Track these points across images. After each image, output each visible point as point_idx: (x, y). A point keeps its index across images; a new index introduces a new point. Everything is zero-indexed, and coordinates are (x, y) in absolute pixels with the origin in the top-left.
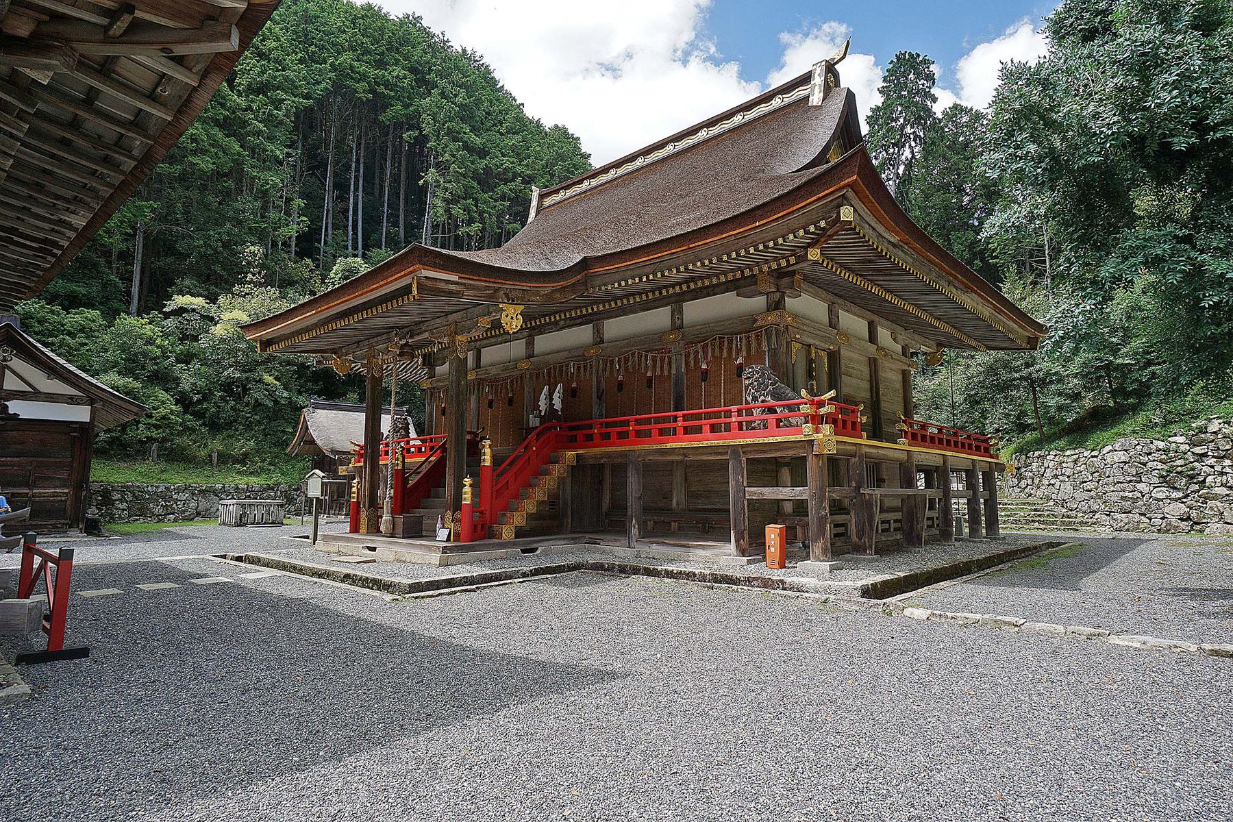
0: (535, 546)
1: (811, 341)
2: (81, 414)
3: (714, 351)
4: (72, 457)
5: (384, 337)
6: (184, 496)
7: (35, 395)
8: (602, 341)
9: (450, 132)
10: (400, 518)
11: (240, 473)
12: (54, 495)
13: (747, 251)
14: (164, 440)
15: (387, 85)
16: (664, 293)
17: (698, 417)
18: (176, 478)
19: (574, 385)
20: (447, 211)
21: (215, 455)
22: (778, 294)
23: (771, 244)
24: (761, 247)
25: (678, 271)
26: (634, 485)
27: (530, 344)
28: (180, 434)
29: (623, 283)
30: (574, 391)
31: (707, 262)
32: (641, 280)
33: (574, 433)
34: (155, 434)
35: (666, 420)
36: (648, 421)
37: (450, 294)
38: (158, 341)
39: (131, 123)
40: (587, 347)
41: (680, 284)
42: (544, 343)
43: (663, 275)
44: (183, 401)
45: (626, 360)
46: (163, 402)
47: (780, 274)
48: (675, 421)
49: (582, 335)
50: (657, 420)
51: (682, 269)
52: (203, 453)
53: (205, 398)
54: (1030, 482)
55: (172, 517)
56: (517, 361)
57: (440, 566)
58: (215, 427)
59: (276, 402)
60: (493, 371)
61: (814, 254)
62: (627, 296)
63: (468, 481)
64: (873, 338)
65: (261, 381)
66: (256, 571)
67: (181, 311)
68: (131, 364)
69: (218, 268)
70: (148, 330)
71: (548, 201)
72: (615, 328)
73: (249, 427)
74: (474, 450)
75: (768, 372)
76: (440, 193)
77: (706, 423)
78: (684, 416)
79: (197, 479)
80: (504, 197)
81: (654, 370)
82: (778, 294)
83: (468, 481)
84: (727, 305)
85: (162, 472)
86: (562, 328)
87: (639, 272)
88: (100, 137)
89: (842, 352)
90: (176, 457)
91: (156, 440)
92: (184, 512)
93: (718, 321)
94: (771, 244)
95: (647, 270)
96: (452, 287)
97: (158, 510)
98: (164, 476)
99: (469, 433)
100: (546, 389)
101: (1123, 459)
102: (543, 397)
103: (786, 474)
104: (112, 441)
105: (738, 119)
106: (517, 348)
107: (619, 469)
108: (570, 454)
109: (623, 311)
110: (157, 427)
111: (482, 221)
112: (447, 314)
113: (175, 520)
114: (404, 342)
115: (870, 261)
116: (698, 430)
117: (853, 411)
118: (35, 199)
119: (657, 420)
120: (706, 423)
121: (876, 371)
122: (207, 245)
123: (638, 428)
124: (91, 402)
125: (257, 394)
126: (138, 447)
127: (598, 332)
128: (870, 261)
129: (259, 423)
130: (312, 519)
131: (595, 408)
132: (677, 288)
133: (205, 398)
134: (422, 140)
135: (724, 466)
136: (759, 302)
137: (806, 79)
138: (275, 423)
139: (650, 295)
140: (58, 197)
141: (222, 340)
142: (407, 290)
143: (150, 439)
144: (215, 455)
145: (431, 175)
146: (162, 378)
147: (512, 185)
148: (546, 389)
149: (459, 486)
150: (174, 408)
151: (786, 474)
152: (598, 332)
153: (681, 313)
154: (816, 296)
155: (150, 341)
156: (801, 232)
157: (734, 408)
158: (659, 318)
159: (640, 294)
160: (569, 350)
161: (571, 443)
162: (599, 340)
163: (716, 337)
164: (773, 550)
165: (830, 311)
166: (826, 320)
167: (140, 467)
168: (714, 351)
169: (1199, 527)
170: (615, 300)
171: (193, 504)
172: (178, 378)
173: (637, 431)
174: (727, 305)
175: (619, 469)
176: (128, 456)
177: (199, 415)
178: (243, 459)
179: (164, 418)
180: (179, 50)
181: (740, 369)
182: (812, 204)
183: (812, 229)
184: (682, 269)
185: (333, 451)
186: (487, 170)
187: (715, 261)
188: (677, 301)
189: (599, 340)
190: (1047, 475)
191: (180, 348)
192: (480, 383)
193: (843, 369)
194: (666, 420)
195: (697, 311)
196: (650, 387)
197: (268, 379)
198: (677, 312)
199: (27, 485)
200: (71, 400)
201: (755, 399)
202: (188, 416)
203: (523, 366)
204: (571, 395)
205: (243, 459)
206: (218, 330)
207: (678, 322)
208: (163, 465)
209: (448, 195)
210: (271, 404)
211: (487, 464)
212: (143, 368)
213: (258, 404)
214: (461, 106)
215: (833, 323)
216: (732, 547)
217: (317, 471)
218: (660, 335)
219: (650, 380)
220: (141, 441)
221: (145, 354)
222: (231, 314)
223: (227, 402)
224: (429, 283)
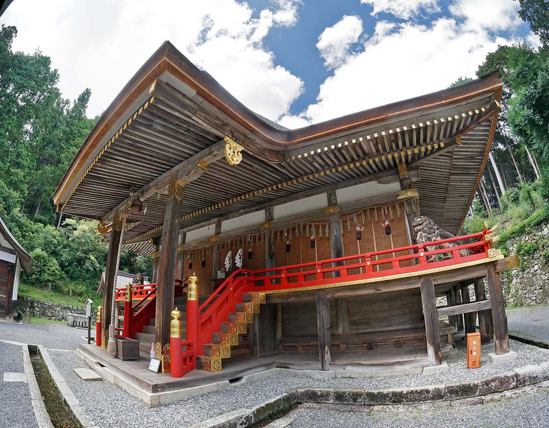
3: (385, 212)
8: (272, 219)
11: (79, 301)
14: (53, 282)
18: (56, 300)
19: (250, 250)
21: (71, 291)
30: (250, 255)
34: (51, 278)
38: (57, 237)
40: (262, 225)
44: (62, 265)
45: (294, 229)
46: (54, 264)
49: (257, 217)
52: (66, 290)
55: (54, 318)
58: (72, 278)
59: (94, 269)
60: (193, 245)
63: (176, 313)
65: (90, 259)
68: (46, 246)
70: (55, 233)
72: (281, 211)
73: (84, 280)
74: (180, 291)
79: (63, 301)
81: (317, 233)
83: (176, 313)
85: (52, 296)
86: (241, 214)
90: (57, 289)
91: (50, 281)
92: (58, 316)
97: (49, 314)
98: (52, 298)
100: (229, 254)
102: (227, 259)
104: (37, 279)
107: (309, 307)
108: (262, 294)
110: (51, 275)
113: (55, 320)
125: (87, 264)
126: (44, 283)
129: (88, 279)
131: (268, 266)
138: (94, 280)
141: (77, 238)
143: (49, 280)
144: (71, 291)
146: (54, 253)
148: (229, 254)
150: (57, 267)
153: (335, 195)
155: (54, 237)
158: (319, 200)
161: (259, 285)
162: (270, 218)
167: (45, 292)
168: (385, 212)
171: (61, 313)
172: (62, 255)
175: (309, 307)
176: (42, 287)
177: (67, 272)
178: (80, 294)
179: (53, 271)
189: (270, 218)
192: (184, 253)
195: (346, 194)
196: (313, 247)
197: (92, 258)
202: (63, 272)
204: (248, 257)
205: (80, 294)
206: (76, 233)
208: (52, 293)
210: (92, 270)
212: (50, 248)
213: (88, 270)
218: (321, 211)
219: (313, 242)
220: (46, 282)
223: (77, 268)
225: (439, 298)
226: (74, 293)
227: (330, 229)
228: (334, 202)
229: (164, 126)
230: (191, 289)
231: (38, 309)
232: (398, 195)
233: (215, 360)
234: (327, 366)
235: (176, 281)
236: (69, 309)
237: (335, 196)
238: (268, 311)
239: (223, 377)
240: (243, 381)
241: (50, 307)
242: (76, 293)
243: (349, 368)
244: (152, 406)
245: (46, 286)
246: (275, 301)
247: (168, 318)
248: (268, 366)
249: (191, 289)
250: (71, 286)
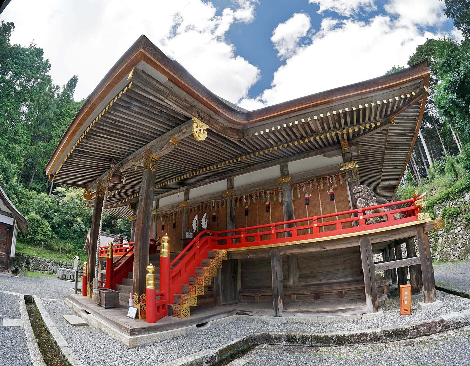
3: (329, 181)
8: (233, 187)
11: (68, 257)
14: (46, 241)
18: (48, 257)
19: (214, 214)
21: (61, 249)
30: (214, 218)
34: (43, 238)
38: (49, 203)
40: (224, 192)
44: (53, 227)
45: (251, 196)
46: (46, 226)
49: (220, 186)
52: (56, 248)
55: (46, 272)
57: (130, 347)
58: (62, 238)
59: (81, 230)
60: (165, 209)
63: (150, 268)
65: (77, 221)
68: (39, 210)
70: (47, 199)
72: (241, 180)
73: (72, 239)
74: (154, 249)
79: (54, 258)
81: (272, 199)
83: (150, 268)
85: (44, 253)
86: (207, 183)
90: (49, 247)
91: (43, 240)
92: (50, 270)
97: (42, 268)
98: (44, 255)
99: (151, 240)
100: (196, 217)
102: (194, 221)
104: (32, 239)
107: (265, 263)
110: (44, 235)
113: (47, 273)
125: (75, 226)
126: (38, 242)
129: (76, 238)
131: (229, 227)
138: (80, 239)
141: (66, 203)
143: (42, 240)
144: (61, 249)
146: (46, 217)
148: (196, 217)
149: (144, 272)
150: (49, 228)
153: (287, 167)
155: (46, 202)
158: (273, 171)
161: (222, 244)
162: (231, 186)
167: (39, 250)
168: (329, 181)
171: (52, 268)
172: (53, 218)
173: (246, 238)
175: (265, 263)
176: (36, 245)
177: (57, 233)
178: (69, 252)
179: (46, 232)
189: (231, 186)
192: (158, 216)
195: (296, 166)
196: (268, 211)
197: (79, 220)
202: (54, 233)
204: (212, 219)
205: (69, 252)
206: (65, 199)
208: (45, 251)
210: (79, 230)
212: (43, 212)
213: (75, 231)
218: (275, 181)
219: (268, 207)
220: (40, 241)
223: (66, 229)
225: (376, 255)
226: (63, 251)
227: (282, 196)
228: (286, 172)
229: (141, 108)
230: (163, 248)
231: (32, 265)
232: (341, 167)
234: (280, 313)
236: (59, 264)
237: (287, 167)
240: (208, 326)
241: (43, 263)
242: (65, 250)
243: (299, 314)
245: (40, 244)
246: (235, 257)
248: (230, 313)
249: (163, 248)
250: (61, 245)
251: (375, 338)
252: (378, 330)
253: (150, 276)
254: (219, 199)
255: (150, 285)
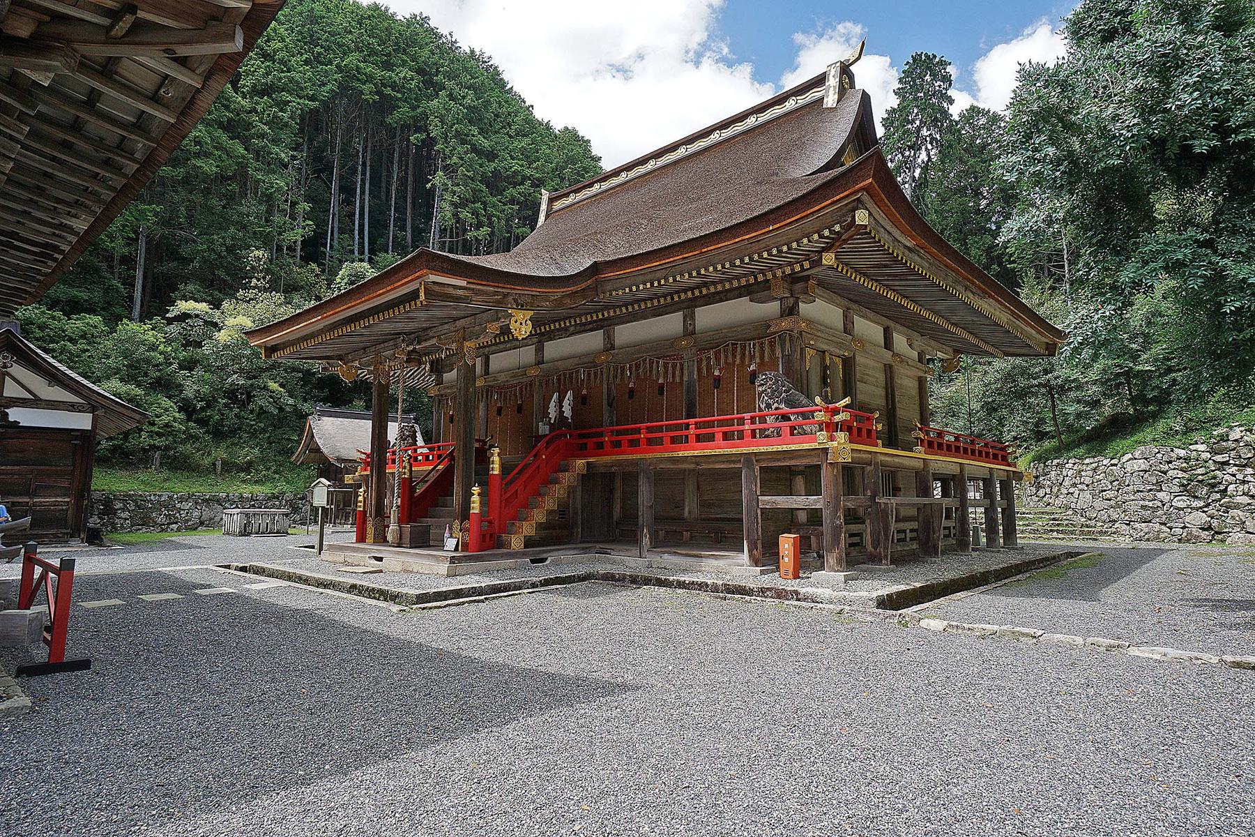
0: (544, 556)
1: (825, 347)
2: (83, 422)
3: (726, 357)
4: (74, 465)
5: (391, 343)
6: (187, 505)
7: (35, 402)
8: (613, 347)
9: (458, 134)
10: (407, 528)
11: (244, 481)
12: (55, 504)
13: (760, 256)
14: (167, 448)
15: (394, 86)
16: (676, 299)
17: (710, 424)
18: (180, 487)
19: (584, 392)
20: (455, 215)
21: (219, 464)
22: (792, 300)
23: (785, 248)
24: (775, 252)
25: (690, 276)
26: (645, 494)
27: (540, 350)
28: (183, 442)
29: (634, 288)
30: (584, 398)
31: (719, 267)
32: (652, 285)
33: (585, 441)
34: (158, 442)
35: (678, 427)
36: (660, 429)
37: (458, 299)
38: (161, 347)
39: (134, 125)
40: (598, 354)
41: (692, 289)
42: (554, 349)
43: (675, 280)
44: (187, 408)
45: (638, 366)
46: (166, 410)
47: (794, 279)
48: (687, 428)
49: (592, 341)
50: (669, 428)
51: (694, 274)
52: (207, 461)
53: (209, 406)
54: (1048, 490)
55: (175, 526)
56: (526, 367)
58: (219, 434)
59: (281, 409)
60: (502, 378)
61: (829, 259)
62: (638, 301)
63: (476, 490)
64: (888, 344)
65: (265, 388)
66: (260, 581)
67: (184, 317)
68: (134, 371)
69: (221, 273)
70: (150, 336)
71: (558, 205)
72: (626, 333)
73: (253, 435)
74: (482, 458)
75: (782, 379)
76: (447, 196)
77: (718, 431)
78: (696, 423)
79: (201, 488)
80: (513, 201)
81: (666, 377)
82: (792, 300)
83: (476, 490)
84: (740, 310)
85: (165, 480)
86: (572, 334)
87: (650, 276)
88: (101, 139)
89: (857, 358)
90: (179, 465)
91: (158, 448)
92: (187, 521)
93: (731, 327)
94: (785, 248)
95: (659, 275)
96: (460, 292)
97: (161, 519)
98: (167, 485)
100: (555, 396)
101: (1143, 467)
102: (552, 404)
103: (800, 482)
104: (114, 449)
105: (751, 121)
106: (527, 355)
108: (580, 462)
109: (634, 317)
110: (159, 435)
111: (490, 225)
112: (455, 319)
113: (179, 530)
114: (411, 348)
115: (885, 266)
116: (711, 438)
117: (868, 419)
118: (36, 202)
119: (669, 428)
120: (718, 431)
121: (892, 378)
122: (210, 250)
123: (650, 435)
124: (93, 409)
125: (261, 401)
126: (140, 455)
127: (609, 338)
128: (885, 266)
129: (264, 430)
130: (317, 528)
131: (606, 416)
132: (689, 294)
133: (209, 406)
134: (430, 142)
135: (736, 474)
136: (773, 308)
137: (820, 80)
138: (280, 431)
139: (662, 301)
140: (59, 201)
141: (226, 347)
142: (414, 295)
143: (153, 447)
144: (219, 464)
145: (439, 178)
146: (165, 385)
147: (521, 188)
148: (555, 396)
150: (177, 415)
151: (800, 482)
152: (609, 338)
153: (693, 318)
154: (830, 301)
155: (153, 348)
156: (816, 237)
157: (747, 416)
158: (671, 324)
159: (651, 299)
160: (579, 356)
161: (582, 451)
162: (610, 346)
163: (729, 343)
164: (786, 560)
165: (845, 316)
166: (841, 326)
167: (143, 475)
168: (726, 357)
169: (1220, 537)
170: (626, 306)
171: (196, 513)
172: (181, 385)
173: (648, 439)
174: (740, 310)
176: (131, 464)
177: (202, 423)
178: (247, 467)
179: (167, 425)
180: (183, 51)
181: (753, 376)
182: (826, 207)
183: (826, 233)
184: (694, 274)
185: (339, 460)
186: (496, 173)
187: (727, 265)
188: (689, 307)
189: (610, 346)
190: (1066, 483)
191: (183, 354)
192: (489, 390)
193: (858, 375)
194: (678, 427)
195: (709, 317)
196: (662, 394)
197: (273, 386)
198: (689, 317)
199: (27, 494)
200: (72, 407)
201: (769, 406)
202: (191, 424)
203: (532, 372)
204: (581, 402)
205: (247, 467)
206: (222, 336)
207: (690, 328)
208: (166, 474)
209: (456, 199)
210: (276, 412)
211: (496, 472)
212: (146, 375)
213: (262, 412)
214: (469, 108)
215: (848, 329)
216: (745, 557)
217: (323, 480)
218: (672, 341)
219: (661, 387)
220: (143, 449)
221: (148, 361)
222: (235, 320)
223: (231, 409)
224: (437, 288)
233: (516, 542)
235: (477, 441)
238: (590, 476)
239: (524, 555)
244: (448, 576)
247: (468, 495)
251: (715, 589)
252: (720, 582)
253: (476, 498)
254: (589, 362)
255: (475, 507)
